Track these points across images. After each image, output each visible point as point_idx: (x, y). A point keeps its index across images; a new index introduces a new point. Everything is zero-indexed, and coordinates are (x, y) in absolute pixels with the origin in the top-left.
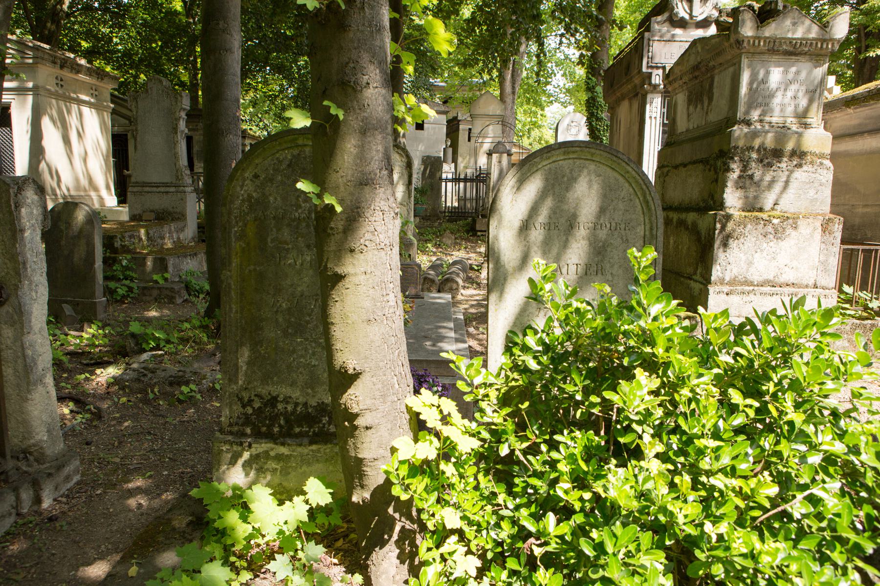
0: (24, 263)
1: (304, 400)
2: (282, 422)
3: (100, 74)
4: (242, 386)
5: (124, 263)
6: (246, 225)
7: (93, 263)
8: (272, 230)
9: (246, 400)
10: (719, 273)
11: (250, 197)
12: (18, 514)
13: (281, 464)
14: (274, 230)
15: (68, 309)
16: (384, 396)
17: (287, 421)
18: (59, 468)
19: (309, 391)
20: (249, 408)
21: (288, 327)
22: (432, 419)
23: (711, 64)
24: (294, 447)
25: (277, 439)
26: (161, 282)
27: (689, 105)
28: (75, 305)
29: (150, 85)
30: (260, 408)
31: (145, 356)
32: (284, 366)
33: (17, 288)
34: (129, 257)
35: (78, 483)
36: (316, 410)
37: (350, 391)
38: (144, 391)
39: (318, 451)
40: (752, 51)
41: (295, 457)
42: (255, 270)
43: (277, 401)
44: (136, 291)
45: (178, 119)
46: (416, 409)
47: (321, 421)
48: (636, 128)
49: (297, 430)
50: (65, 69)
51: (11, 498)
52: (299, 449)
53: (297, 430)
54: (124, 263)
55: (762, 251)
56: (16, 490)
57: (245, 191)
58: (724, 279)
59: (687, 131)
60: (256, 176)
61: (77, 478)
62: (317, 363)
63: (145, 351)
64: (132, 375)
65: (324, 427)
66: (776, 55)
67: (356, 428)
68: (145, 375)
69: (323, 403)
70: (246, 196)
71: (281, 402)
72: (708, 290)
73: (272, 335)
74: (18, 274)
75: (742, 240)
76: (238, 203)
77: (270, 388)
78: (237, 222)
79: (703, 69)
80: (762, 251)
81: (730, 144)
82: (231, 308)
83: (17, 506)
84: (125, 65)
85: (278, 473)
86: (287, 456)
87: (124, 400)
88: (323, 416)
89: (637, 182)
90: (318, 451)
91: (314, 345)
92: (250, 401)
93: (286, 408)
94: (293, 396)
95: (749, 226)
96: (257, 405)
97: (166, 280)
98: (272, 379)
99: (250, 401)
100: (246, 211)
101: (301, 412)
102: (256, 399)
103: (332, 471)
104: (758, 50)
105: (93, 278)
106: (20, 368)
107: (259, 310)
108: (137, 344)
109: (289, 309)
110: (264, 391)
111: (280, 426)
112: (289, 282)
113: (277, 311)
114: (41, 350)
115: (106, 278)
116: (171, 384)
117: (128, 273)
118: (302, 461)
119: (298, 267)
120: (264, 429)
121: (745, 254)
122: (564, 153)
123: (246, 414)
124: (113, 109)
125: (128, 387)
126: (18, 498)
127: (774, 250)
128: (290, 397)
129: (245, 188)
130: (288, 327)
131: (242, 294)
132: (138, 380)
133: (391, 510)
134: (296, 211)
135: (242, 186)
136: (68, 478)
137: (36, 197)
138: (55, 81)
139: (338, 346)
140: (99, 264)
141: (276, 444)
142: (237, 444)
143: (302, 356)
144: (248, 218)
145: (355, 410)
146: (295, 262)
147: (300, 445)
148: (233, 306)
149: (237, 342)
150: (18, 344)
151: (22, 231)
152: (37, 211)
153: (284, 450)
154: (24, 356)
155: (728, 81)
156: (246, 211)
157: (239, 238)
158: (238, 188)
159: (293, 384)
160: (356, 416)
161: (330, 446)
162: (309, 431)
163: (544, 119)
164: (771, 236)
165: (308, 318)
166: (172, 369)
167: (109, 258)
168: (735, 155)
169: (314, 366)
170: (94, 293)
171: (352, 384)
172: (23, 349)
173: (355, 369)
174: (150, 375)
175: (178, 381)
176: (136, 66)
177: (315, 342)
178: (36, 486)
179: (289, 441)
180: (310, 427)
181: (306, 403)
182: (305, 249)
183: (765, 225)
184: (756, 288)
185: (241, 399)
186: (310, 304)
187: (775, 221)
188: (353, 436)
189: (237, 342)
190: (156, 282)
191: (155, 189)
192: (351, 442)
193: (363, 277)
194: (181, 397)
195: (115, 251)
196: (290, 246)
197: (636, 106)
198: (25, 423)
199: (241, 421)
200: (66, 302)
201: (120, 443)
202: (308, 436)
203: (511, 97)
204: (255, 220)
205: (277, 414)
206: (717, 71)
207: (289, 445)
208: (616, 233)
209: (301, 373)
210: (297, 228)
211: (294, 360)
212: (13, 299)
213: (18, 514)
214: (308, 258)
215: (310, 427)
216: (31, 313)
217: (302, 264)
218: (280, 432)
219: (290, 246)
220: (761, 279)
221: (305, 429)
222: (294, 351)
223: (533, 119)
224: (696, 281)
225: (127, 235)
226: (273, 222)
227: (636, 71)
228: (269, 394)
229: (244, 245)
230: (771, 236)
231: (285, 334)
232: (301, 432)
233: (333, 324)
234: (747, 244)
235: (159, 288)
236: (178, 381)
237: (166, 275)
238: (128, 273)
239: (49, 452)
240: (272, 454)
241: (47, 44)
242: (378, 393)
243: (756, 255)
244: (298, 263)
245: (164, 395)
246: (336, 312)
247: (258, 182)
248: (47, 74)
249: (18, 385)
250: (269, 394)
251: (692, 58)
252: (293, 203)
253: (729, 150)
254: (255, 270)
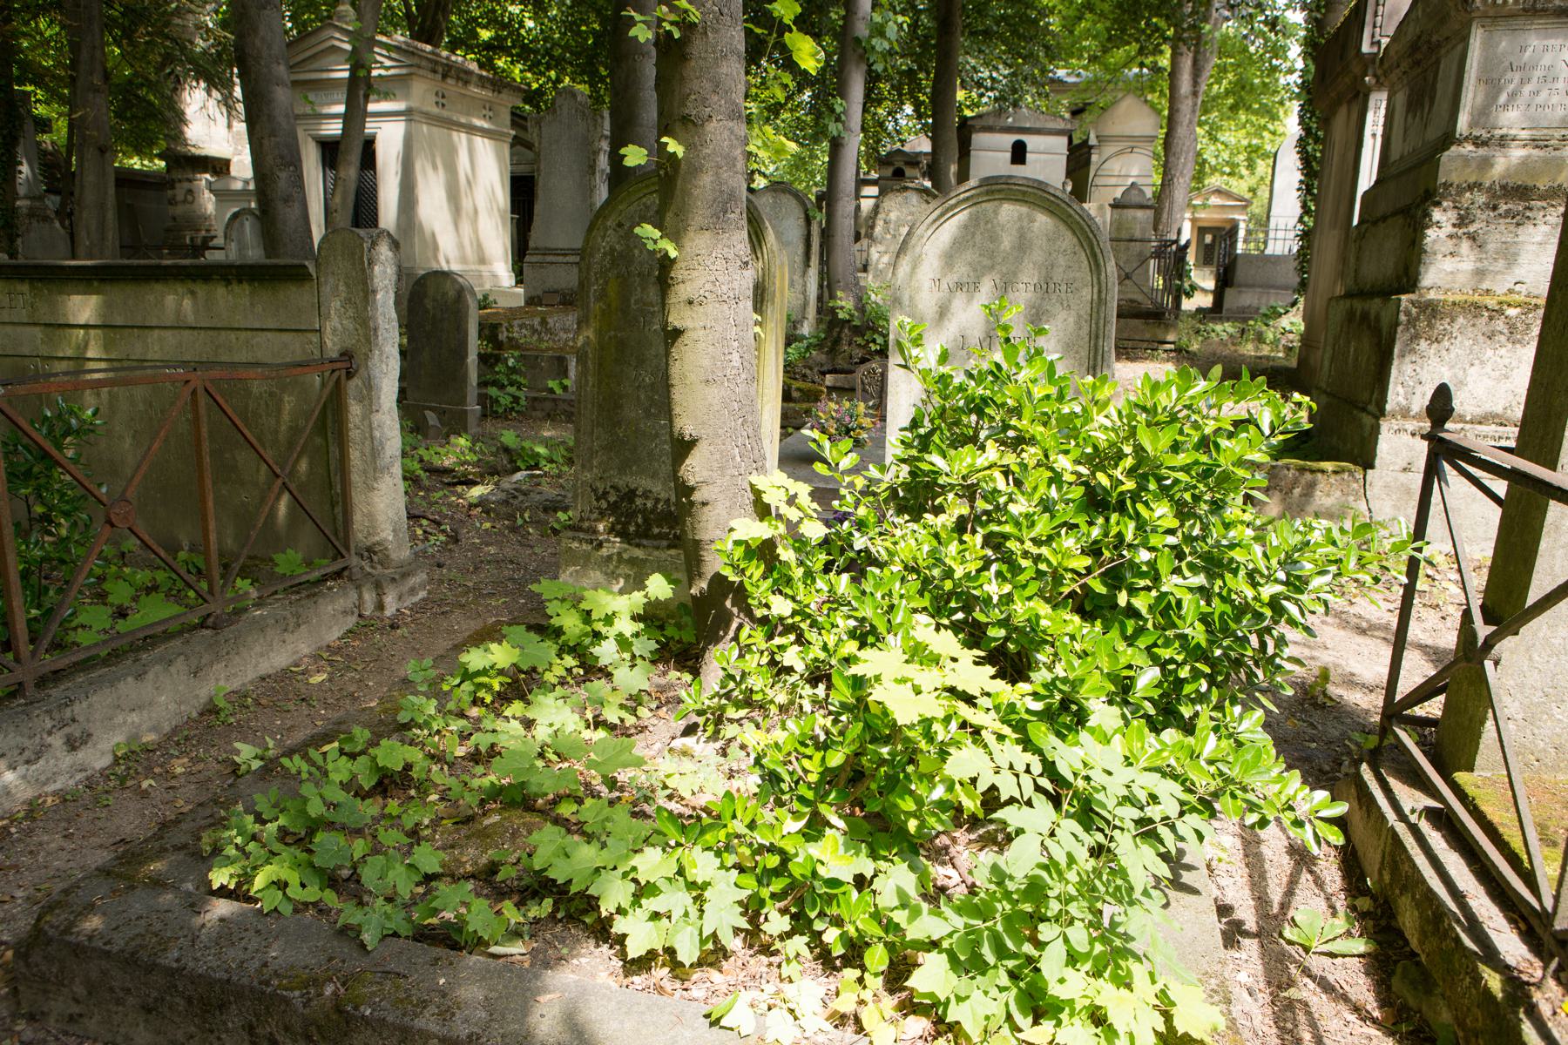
0: (376, 330)
2: (640, 521)
3: (500, 83)
5: (511, 362)
6: (606, 283)
7: (465, 356)
10: (1401, 399)
11: (612, 249)
12: (360, 616)
15: (432, 418)
16: (722, 468)
17: (645, 520)
18: (405, 575)
22: (773, 498)
23: (1435, 38)
26: (559, 391)
27: (1408, 111)
28: (441, 413)
29: (559, 101)
31: (519, 476)
33: (367, 357)
34: (516, 354)
35: (423, 599)
37: (688, 462)
38: (512, 517)
40: (1491, 13)
44: (523, 402)
45: (596, 153)
46: (760, 487)
48: (1351, 155)
49: (656, 531)
50: (449, 81)
51: (353, 595)
52: (656, 553)
53: (656, 531)
54: (511, 362)
55: (1482, 362)
56: (358, 587)
58: (1408, 410)
59: (1402, 157)
60: (620, 225)
61: (422, 594)
63: (519, 469)
64: (501, 496)
66: (1541, 17)
67: (692, 504)
68: (515, 497)
72: (1378, 426)
74: (369, 341)
75: (1446, 343)
76: (598, 256)
77: (628, 479)
79: (1425, 48)
80: (1482, 362)
81: (1436, 179)
83: (359, 605)
84: (539, 63)
87: (488, 525)
89: (1082, 228)
92: (605, 494)
95: (1461, 320)
96: (612, 499)
97: (565, 388)
99: (605, 494)
104: (1505, 11)
105: (464, 378)
106: (367, 450)
108: (512, 461)
109: (652, 385)
110: (622, 482)
111: (637, 525)
114: (389, 434)
115: (483, 384)
116: (546, 510)
117: (514, 377)
121: (1452, 367)
122: (987, 193)
124: (515, 137)
125: (494, 510)
126: (360, 597)
127: (1507, 361)
131: (600, 365)
132: (506, 502)
133: (728, 604)
135: (603, 237)
136: (413, 591)
137: (390, 254)
138: (434, 99)
139: (677, 410)
140: (472, 359)
145: (691, 483)
147: (657, 548)
150: (366, 423)
151: (374, 292)
152: (391, 270)
153: (639, 553)
154: (372, 438)
155: (1454, 67)
157: (598, 299)
159: (654, 476)
160: (693, 489)
163: (1278, 140)
164: (1503, 338)
166: (549, 491)
167: (491, 355)
168: (1444, 197)
170: (465, 397)
172: (371, 429)
174: (521, 498)
175: (552, 507)
176: (558, 63)
178: (378, 587)
179: (645, 542)
180: (671, 528)
183: (1491, 318)
184: (1468, 426)
185: (595, 490)
187: (1512, 312)
188: (690, 515)
190: (551, 391)
191: (560, 259)
192: (689, 519)
193: (702, 332)
194: (557, 526)
195: (499, 345)
197: (1354, 116)
198: (371, 516)
200: (431, 409)
201: (476, 568)
203: (1190, 102)
206: (1443, 51)
208: (1054, 297)
212: (362, 371)
213: (360, 616)
215: (671, 528)
216: (380, 389)
218: (637, 532)
220: (1479, 411)
223: (1254, 142)
224: (1369, 413)
225: (516, 323)
227: (1353, 52)
230: (1503, 338)
231: (647, 412)
234: (1455, 351)
235: (554, 400)
236: (552, 507)
237: (566, 382)
238: (514, 377)
239: (394, 556)
240: (625, 556)
241: (427, 42)
242: (715, 465)
243: (1472, 370)
245: (536, 523)
246: (675, 370)
247: (622, 233)
248: (422, 93)
249: (365, 472)
251: (1411, 29)
253: (1435, 190)
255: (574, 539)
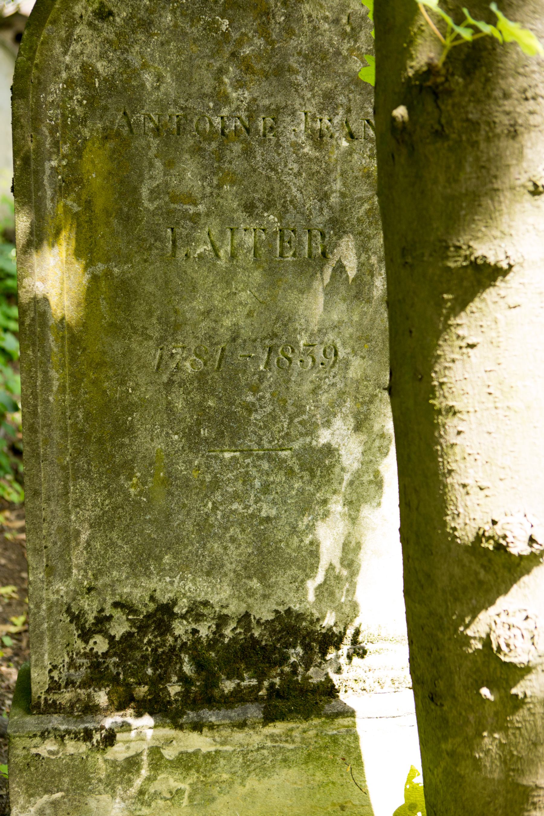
1: (242, 609)
2: (187, 669)
4: (79, 583)
6: (79, 152)
8: (151, 165)
9: (91, 618)
13: (193, 777)
14: (158, 163)
19: (255, 583)
20: (98, 638)
21: (199, 423)
24: (226, 732)
25: (180, 713)
30: (128, 636)
32: (189, 526)
36: (273, 631)
39: (288, 736)
41: (228, 757)
42: (108, 274)
43: (173, 616)
47: (285, 658)
49: (228, 686)
52: (239, 736)
53: (228, 686)
57: (76, 56)
62: (273, 512)
65: (294, 672)
69: (289, 611)
70: (76, 70)
71: (183, 617)
73: (159, 445)
77: (154, 583)
78: (56, 144)
82: (47, 380)
85: (185, 801)
86: (208, 755)
88: (288, 645)
90: (288, 736)
91: (265, 466)
93: (195, 631)
94: (214, 599)
98: (159, 559)
100: (79, 111)
101: (234, 640)
102: (118, 614)
103: (321, 785)
107: (123, 383)
109: (201, 377)
111: (184, 679)
112: (199, 304)
113: (170, 382)
118: (246, 765)
119: (223, 263)
120: (142, 690)
123: (91, 655)
128: (206, 604)
129: (76, 47)
130: (199, 423)
134: (217, 110)
135: (67, 42)
141: (180, 727)
142: (76, 737)
143: (236, 496)
144: (86, 133)
146: (215, 250)
147: (242, 725)
148: (54, 374)
149: (64, 468)
156: (79, 111)
158: (58, 49)
161: (316, 721)
162: (259, 687)
165: (250, 398)
169: (268, 519)
171: (514, 580)
173: (532, 541)
177: (270, 459)
180: (261, 676)
181: (247, 615)
182: (240, 215)
186: (256, 359)
189: (64, 468)
196: (201, 208)
199: (79, 676)
202: (257, 699)
204: (106, 138)
205: (173, 649)
207: (212, 727)
209: (233, 540)
210: (220, 159)
211: (215, 508)
214: (250, 240)
215: (261, 676)
217: (233, 256)
218: (185, 694)
219: (201, 208)
221: (250, 682)
222: (216, 484)
226: (155, 143)
228: (152, 598)
229: (76, 208)
232: (238, 690)
233: (452, 411)
240: (169, 753)
244: (224, 252)
250: (152, 598)
252: (207, 90)
254: (108, 274)
255: (44, 735)
